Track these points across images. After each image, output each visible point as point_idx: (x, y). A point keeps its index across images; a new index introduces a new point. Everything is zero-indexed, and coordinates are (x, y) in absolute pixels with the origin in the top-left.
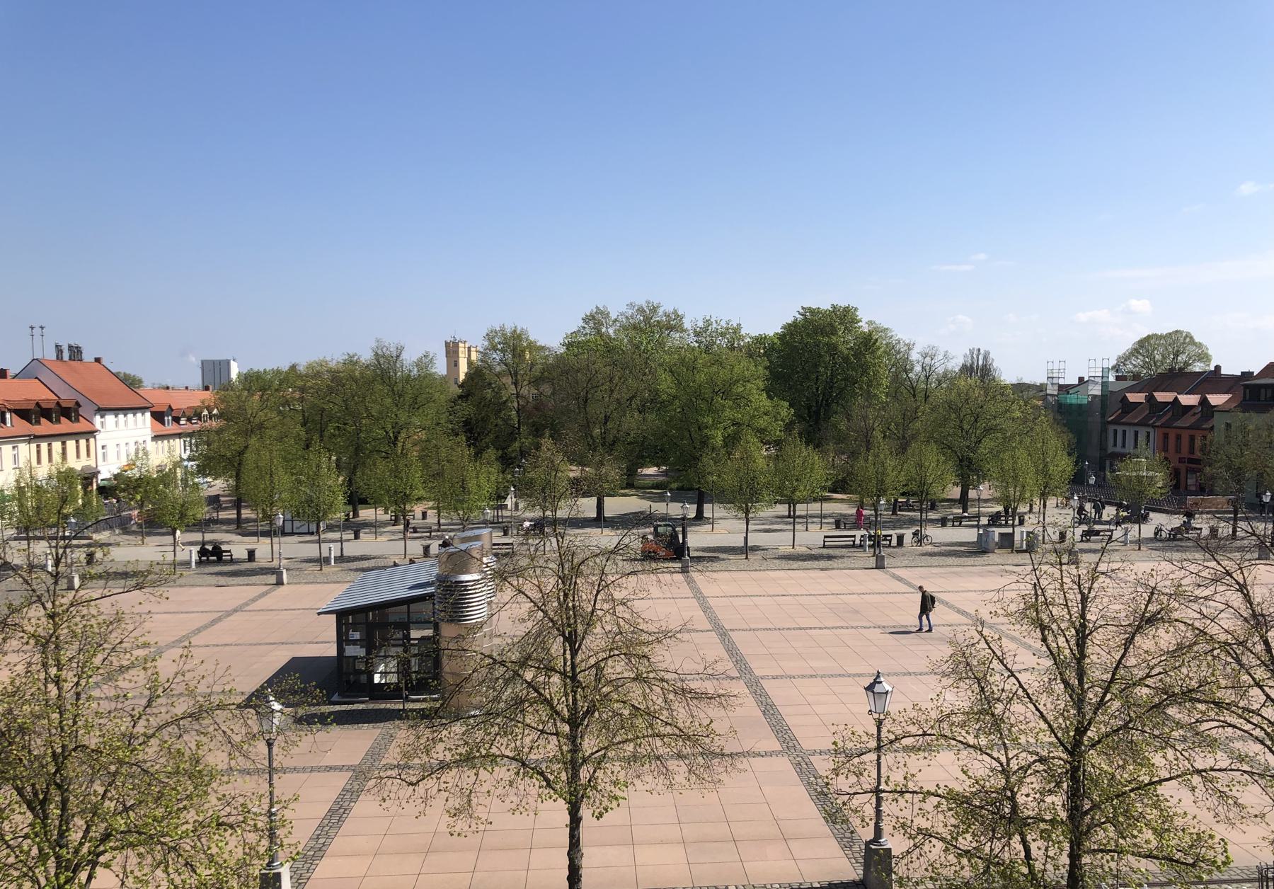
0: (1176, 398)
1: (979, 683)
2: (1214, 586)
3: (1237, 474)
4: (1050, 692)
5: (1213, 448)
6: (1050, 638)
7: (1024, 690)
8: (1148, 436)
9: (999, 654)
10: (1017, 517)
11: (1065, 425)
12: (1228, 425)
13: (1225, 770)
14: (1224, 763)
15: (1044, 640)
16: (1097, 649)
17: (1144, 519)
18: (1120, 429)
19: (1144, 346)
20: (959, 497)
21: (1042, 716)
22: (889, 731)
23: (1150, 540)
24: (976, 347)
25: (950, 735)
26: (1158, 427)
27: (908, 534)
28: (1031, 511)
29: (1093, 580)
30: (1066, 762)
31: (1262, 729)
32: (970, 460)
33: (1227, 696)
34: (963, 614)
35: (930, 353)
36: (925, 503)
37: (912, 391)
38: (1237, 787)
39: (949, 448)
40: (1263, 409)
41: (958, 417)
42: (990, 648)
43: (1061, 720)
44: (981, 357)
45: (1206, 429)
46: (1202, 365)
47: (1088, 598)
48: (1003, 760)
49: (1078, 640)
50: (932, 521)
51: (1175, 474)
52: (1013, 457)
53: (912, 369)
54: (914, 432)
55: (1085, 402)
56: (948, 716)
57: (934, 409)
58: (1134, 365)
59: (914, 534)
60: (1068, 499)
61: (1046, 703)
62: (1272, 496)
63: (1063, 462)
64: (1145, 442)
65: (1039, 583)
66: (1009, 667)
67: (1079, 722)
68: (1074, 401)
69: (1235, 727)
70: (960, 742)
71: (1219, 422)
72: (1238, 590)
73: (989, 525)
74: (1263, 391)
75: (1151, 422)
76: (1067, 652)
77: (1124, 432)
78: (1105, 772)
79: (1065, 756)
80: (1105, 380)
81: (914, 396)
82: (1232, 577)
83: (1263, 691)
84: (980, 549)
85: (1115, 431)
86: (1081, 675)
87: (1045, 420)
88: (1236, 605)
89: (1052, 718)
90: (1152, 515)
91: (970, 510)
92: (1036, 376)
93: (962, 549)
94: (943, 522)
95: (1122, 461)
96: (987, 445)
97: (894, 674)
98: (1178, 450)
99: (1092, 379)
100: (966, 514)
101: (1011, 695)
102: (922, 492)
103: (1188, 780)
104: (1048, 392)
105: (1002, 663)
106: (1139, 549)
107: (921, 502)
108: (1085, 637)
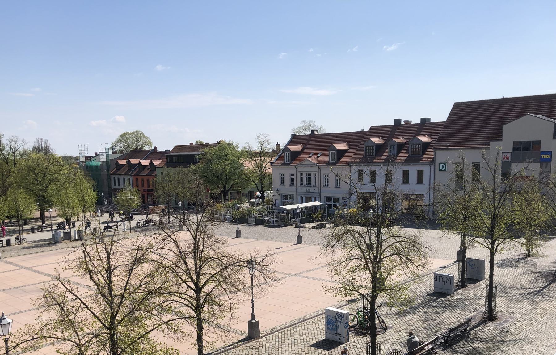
0: (140, 162)
1: (60, 306)
2: (164, 242)
3: (168, 194)
4: (96, 302)
5: (157, 184)
6: (94, 276)
7: (84, 304)
8: (129, 180)
9: (69, 288)
10: (71, 224)
11: (90, 176)
12: (162, 173)
13: (175, 319)
14: (174, 317)
15: (91, 278)
16: (117, 278)
17: (131, 218)
18: (116, 177)
19: (123, 137)
20: (39, 217)
21: (95, 316)
22: (12, 342)
23: (135, 228)
24: (40, 138)
25: (48, 336)
26: (133, 175)
27: (13, 239)
28: (78, 220)
29: (112, 245)
30: (107, 334)
31: (188, 300)
32: (43, 196)
33: (174, 289)
34: (48, 276)
35: (14, 140)
36: (21, 221)
37: (5, 161)
38: (180, 325)
39: (31, 190)
40: (174, 166)
41: (35, 174)
42: (64, 286)
43: (103, 315)
44: (43, 143)
45: (153, 176)
46: (149, 147)
47: (110, 254)
48: (77, 340)
49: (107, 275)
50: (26, 230)
51: (143, 197)
52: (66, 194)
53: (4, 149)
54: (10, 183)
55: (99, 165)
56: (46, 326)
57: (20, 170)
58: (119, 147)
59: (16, 238)
60: (95, 212)
61: (96, 308)
62: (182, 203)
63: (91, 194)
64: (128, 183)
65: (86, 250)
66: (75, 294)
67: (112, 313)
68: (94, 165)
69: (177, 302)
70: (54, 338)
71: (158, 172)
72: (174, 243)
73: (57, 229)
74: (174, 158)
75: (130, 173)
76: (103, 281)
77: (119, 179)
78: (125, 334)
79: (107, 331)
80: (107, 154)
81: (7, 163)
82: (171, 237)
83: (186, 284)
84: (54, 241)
85: (114, 178)
86: (111, 290)
87: (80, 174)
88: (173, 249)
89: (99, 315)
90: (135, 216)
91: (46, 223)
92: (74, 153)
93: (44, 243)
94: (32, 230)
95: (119, 192)
96: (52, 188)
97: (13, 314)
98: (143, 186)
99: (101, 153)
100: (44, 225)
101: (78, 308)
102: (18, 215)
103: (161, 327)
104: (81, 160)
105: (71, 293)
106: (131, 232)
107: (18, 221)
108: (110, 273)
